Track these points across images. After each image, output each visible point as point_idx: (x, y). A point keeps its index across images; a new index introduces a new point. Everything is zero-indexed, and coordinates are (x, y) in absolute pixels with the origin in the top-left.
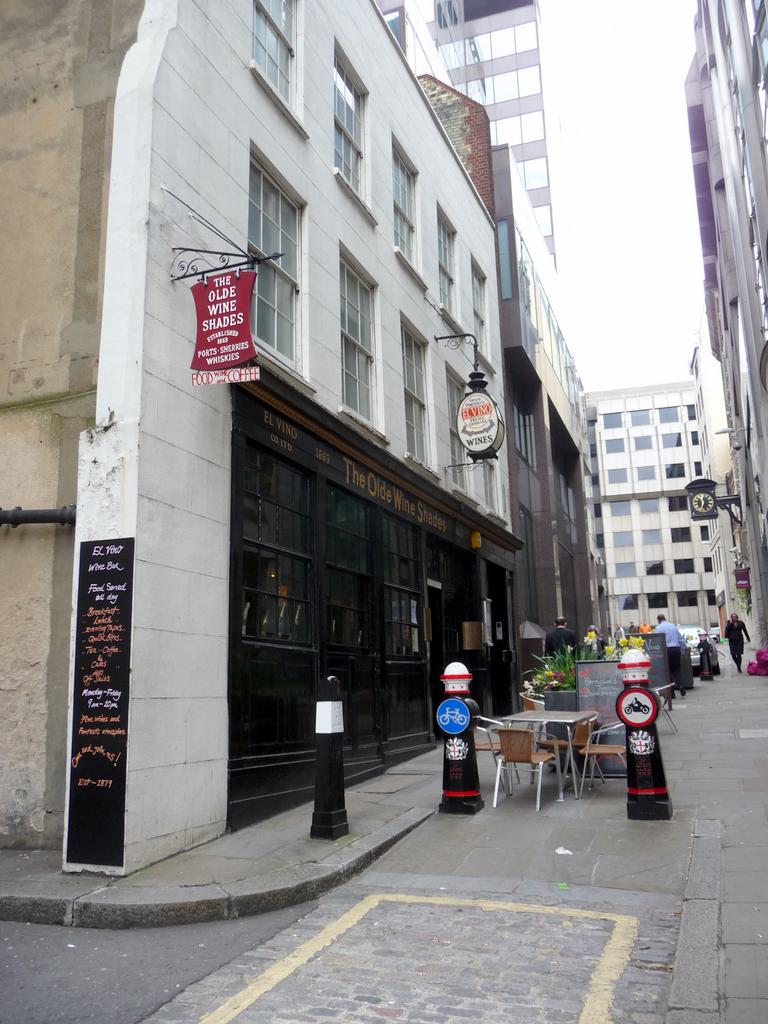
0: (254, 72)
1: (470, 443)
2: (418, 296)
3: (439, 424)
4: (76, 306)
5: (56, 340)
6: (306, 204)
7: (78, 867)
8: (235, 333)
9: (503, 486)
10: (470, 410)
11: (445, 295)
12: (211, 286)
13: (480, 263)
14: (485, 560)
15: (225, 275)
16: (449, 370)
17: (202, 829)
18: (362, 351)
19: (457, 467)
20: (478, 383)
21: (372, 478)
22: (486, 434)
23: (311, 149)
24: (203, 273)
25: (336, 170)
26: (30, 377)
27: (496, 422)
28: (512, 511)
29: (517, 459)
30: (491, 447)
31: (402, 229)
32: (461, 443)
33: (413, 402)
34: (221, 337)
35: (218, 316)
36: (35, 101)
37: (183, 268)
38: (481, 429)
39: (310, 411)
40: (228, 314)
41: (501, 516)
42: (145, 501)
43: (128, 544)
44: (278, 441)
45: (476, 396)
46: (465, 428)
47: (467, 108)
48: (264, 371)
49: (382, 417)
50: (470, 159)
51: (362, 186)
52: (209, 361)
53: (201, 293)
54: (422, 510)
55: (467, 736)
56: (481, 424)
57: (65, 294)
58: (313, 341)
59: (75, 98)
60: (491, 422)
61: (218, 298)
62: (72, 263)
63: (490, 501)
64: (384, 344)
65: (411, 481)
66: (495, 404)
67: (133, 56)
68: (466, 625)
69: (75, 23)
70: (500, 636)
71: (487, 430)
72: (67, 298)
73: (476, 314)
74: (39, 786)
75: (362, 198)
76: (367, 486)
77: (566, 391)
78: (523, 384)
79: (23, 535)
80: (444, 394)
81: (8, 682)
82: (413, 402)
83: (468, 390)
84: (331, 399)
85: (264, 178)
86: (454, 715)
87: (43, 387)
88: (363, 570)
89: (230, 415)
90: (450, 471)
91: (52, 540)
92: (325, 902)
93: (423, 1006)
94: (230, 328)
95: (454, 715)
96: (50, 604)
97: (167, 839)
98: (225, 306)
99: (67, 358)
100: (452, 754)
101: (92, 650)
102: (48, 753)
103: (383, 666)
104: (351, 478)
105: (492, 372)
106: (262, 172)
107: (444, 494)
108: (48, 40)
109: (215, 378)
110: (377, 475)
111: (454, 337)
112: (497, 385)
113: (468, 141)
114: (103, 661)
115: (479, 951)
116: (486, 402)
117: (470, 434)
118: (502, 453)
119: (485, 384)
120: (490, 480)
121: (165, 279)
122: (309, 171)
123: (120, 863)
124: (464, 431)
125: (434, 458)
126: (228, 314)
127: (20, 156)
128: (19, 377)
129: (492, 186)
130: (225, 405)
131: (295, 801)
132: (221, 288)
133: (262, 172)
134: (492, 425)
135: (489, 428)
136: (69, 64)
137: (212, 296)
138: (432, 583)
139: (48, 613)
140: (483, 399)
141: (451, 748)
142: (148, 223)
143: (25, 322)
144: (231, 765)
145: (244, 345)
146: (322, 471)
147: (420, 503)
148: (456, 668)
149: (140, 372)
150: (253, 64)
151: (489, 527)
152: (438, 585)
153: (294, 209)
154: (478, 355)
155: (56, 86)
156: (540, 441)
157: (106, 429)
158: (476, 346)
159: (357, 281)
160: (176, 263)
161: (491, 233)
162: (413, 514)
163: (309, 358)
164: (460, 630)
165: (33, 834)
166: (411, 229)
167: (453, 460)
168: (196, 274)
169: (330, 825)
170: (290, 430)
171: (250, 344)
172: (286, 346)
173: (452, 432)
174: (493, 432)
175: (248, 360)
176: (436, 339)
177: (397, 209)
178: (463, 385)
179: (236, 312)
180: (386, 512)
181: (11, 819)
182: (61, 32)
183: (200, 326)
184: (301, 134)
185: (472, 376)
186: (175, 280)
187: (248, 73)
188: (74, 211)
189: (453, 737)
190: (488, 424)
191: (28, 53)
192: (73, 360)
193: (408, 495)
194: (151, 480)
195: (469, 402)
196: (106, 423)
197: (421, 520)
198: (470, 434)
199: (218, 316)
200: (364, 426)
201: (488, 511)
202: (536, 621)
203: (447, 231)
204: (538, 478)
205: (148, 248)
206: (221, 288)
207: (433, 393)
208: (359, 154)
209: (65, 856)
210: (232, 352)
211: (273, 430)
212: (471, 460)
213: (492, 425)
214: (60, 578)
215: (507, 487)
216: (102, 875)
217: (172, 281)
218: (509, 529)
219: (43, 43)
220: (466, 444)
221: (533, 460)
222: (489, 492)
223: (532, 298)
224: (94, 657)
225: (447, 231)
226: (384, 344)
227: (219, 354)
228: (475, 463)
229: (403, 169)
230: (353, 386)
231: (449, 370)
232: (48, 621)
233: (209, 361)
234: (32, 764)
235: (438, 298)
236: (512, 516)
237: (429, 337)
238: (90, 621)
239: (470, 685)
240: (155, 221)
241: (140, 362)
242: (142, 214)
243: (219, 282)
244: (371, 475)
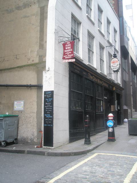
1: (113, 69)
3: (107, 65)
4: (40, 46)
5: (36, 53)
6: (81, 23)
7: (45, 147)
8: (71, 53)
9: (120, 77)
11: (108, 36)
12: (66, 44)
13: (116, 28)
15: (69, 42)
16: (109, 53)
18: (91, 51)
19: (110, 74)
20: (115, 56)
25: (87, 15)
26: (31, 60)
27: (119, 64)
28: (122, 82)
29: (123, 70)
32: (111, 68)
33: (102, 60)
35: (67, 49)
36: (31, 6)
39: (82, 65)
40: (69, 49)
41: (120, 83)
43: (52, 92)
44: (79, 74)
45: (115, 59)
48: (76, 59)
49: (95, 64)
50: (114, 4)
51: (92, 16)
52: (66, 58)
53: (64, 45)
57: (38, 44)
58: (83, 50)
59: (38, 5)
60: (118, 64)
62: (39, 38)
63: (117, 80)
64: (96, 49)
65: (101, 77)
66: (119, 60)
68: (112, 106)
70: (119, 108)
71: (117, 66)
72: (38, 45)
73: (115, 40)
74: (36, 134)
75: (92, 19)
77: (135, 54)
78: (125, 53)
79: (31, 89)
80: (108, 58)
81: (29, 116)
82: (102, 60)
83: (113, 57)
84: (86, 62)
91: (36, 89)
92: (88, 154)
93: (107, 167)
94: (69, 52)
96: (37, 102)
98: (69, 47)
99: (38, 56)
101: (47, 110)
102: (37, 128)
103: (96, 115)
105: (118, 52)
106: (73, 17)
107: (108, 79)
109: (67, 61)
112: (119, 55)
114: (49, 111)
115: (116, 161)
117: (113, 67)
118: (120, 71)
120: (117, 76)
121: (58, 42)
122: (82, 16)
123: (53, 147)
124: (112, 66)
125: (105, 72)
126: (69, 49)
127: (28, 17)
128: (29, 60)
129: (119, 10)
130: (68, 65)
131: (83, 138)
132: (68, 44)
133: (73, 17)
134: (118, 65)
135: (117, 66)
137: (66, 46)
138: (105, 97)
139: (36, 103)
143: (30, 49)
145: (72, 55)
146: (85, 76)
148: (111, 115)
149: (54, 60)
151: (117, 85)
152: (106, 98)
154: (115, 49)
156: (128, 66)
157: (48, 71)
158: (115, 48)
159: (91, 37)
161: (118, 21)
163: (82, 54)
164: (111, 107)
165: (35, 142)
166: (101, 23)
167: (110, 72)
169: (88, 142)
171: (73, 55)
172: (77, 52)
173: (109, 66)
174: (118, 66)
175: (73, 58)
178: (112, 56)
181: (31, 139)
183: (64, 51)
184: (80, 8)
185: (114, 54)
186: (59, 43)
188: (39, 28)
190: (117, 65)
192: (39, 57)
194: (54, 79)
196: (48, 70)
198: (113, 67)
199: (67, 49)
200: (92, 67)
201: (117, 82)
202: (126, 105)
203: (109, 22)
204: (128, 74)
206: (68, 44)
207: (105, 58)
208: (91, 9)
209: (43, 145)
210: (70, 56)
212: (113, 72)
213: (118, 65)
214: (39, 97)
215: (121, 77)
216: (50, 148)
218: (121, 86)
220: (112, 69)
221: (127, 70)
223: (127, 30)
224: (47, 112)
226: (96, 49)
227: (67, 57)
231: (109, 53)
232: (36, 105)
233: (66, 58)
234: (34, 130)
235: (107, 38)
236: (122, 83)
237: (105, 46)
238: (46, 105)
239: (113, 118)
240: (56, 32)
242: (54, 31)
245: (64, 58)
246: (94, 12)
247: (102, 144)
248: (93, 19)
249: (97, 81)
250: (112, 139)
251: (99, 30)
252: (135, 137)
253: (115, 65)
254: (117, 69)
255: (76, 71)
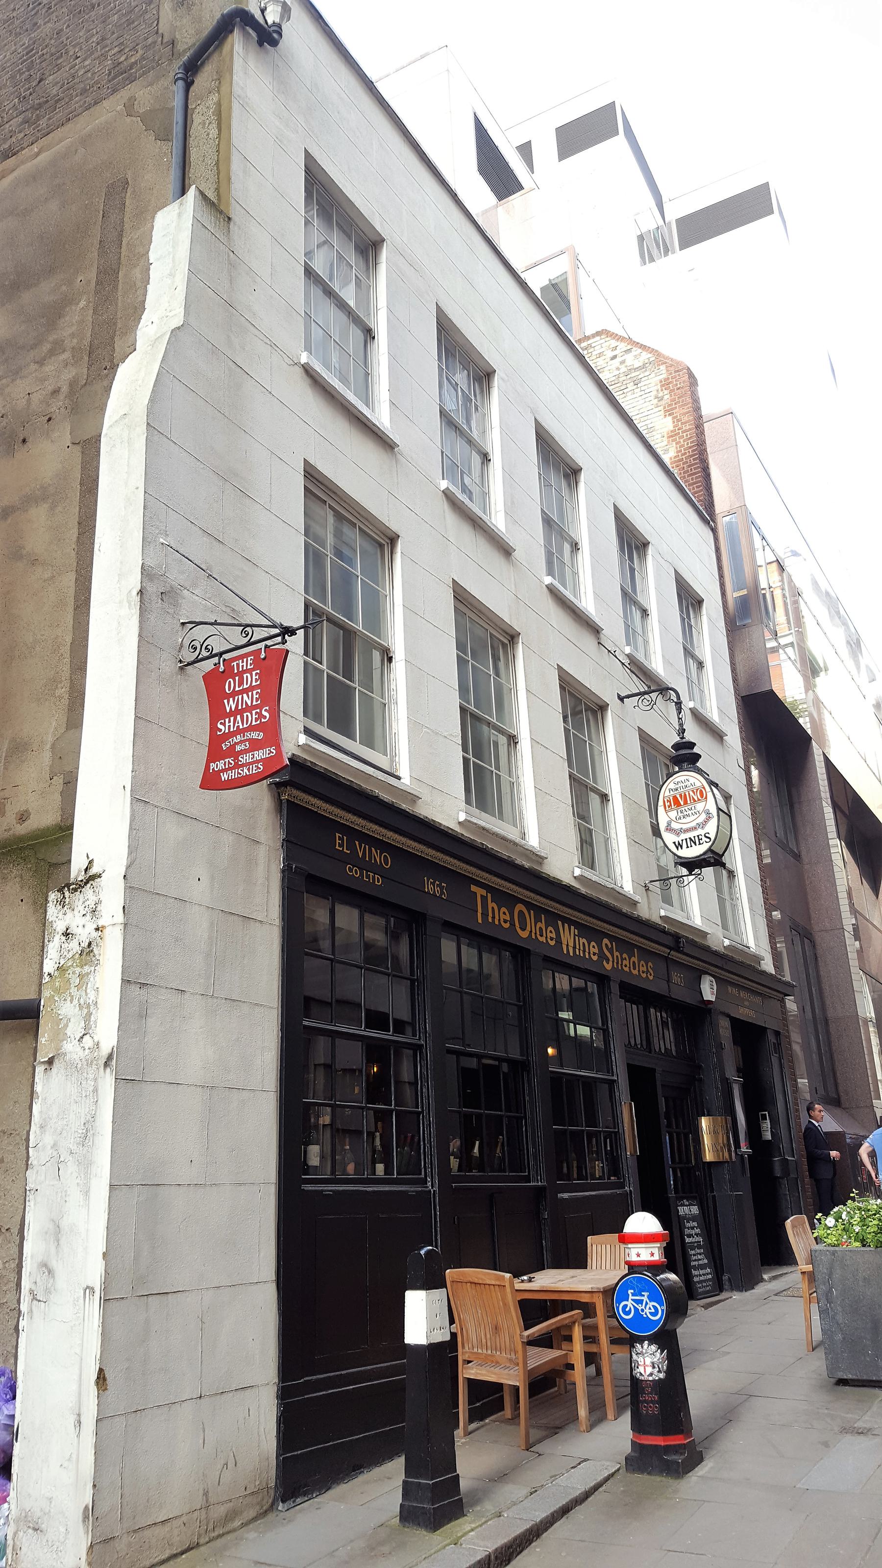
0: (308, 371)
1: (679, 846)
2: (588, 641)
10: (675, 798)
11: (695, 684)
12: (229, 672)
14: (728, 1016)
17: (231, 1504)
21: (521, 912)
22: (700, 832)
23: (399, 456)
24: (221, 654)
25: (548, 580)
27: (714, 811)
30: (710, 850)
31: (561, 550)
34: (241, 742)
36: (24, 441)
37: (195, 649)
38: (693, 824)
40: (249, 709)
42: (135, 989)
46: (669, 824)
47: (663, 367)
49: (537, 823)
52: (224, 777)
53: (214, 684)
54: (611, 951)
55: (665, 1339)
56: (692, 818)
60: (708, 813)
61: (237, 689)
67: (124, 372)
69: (73, 335)
73: (688, 653)
76: (513, 924)
78: (777, 737)
85: (330, 507)
86: (641, 1302)
87: (26, 823)
88: (515, 1054)
89: (279, 844)
90: (656, 887)
94: (251, 728)
95: (641, 1302)
97: (167, 1528)
100: (641, 1369)
104: (485, 915)
108: (41, 363)
110: (529, 905)
111: (645, 693)
113: (669, 412)
116: (698, 784)
119: (698, 757)
121: (169, 666)
122: (400, 494)
124: (669, 829)
125: (623, 874)
126: (249, 709)
132: (241, 674)
135: (706, 822)
136: (65, 389)
137: (230, 685)
140: (692, 780)
141: (640, 1360)
142: (141, 592)
144: (284, 1394)
147: (606, 941)
150: (304, 358)
151: (733, 967)
153: (381, 546)
155: (50, 419)
160: (186, 643)
162: (595, 958)
163: (413, 753)
168: (212, 656)
170: (378, 857)
176: (621, 699)
177: (547, 521)
179: (259, 707)
180: (547, 959)
182: (57, 348)
183: (213, 728)
187: (299, 371)
189: (641, 1340)
190: (703, 817)
191: (18, 381)
193: (585, 931)
195: (672, 786)
197: (608, 967)
198: (677, 833)
199: (237, 712)
203: (632, 543)
205: (141, 628)
206: (241, 674)
211: (353, 859)
212: (685, 871)
217: (181, 668)
218: (768, 965)
219: (36, 366)
220: (674, 849)
222: (732, 915)
225: (632, 543)
227: (237, 766)
228: (690, 874)
229: (557, 468)
230: (483, 780)
231: (645, 739)
237: (607, 695)
240: (153, 589)
241: (128, 788)
242: (134, 581)
243: (238, 665)
244: (520, 907)
245: (211, 782)
246: (508, 475)
247: (565, 1511)
248: (588, 604)
249: (559, 942)
250: (668, 1449)
251: (447, 495)
252: (881, 1410)
253: (690, 821)
254: (705, 847)
255: (355, 873)
